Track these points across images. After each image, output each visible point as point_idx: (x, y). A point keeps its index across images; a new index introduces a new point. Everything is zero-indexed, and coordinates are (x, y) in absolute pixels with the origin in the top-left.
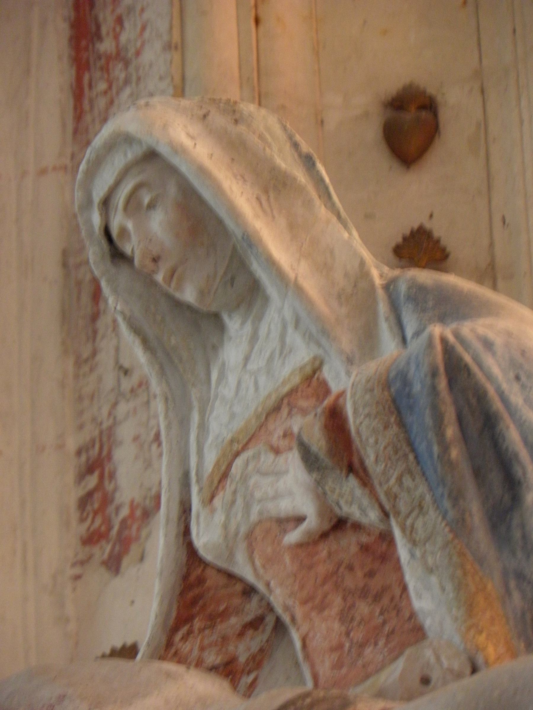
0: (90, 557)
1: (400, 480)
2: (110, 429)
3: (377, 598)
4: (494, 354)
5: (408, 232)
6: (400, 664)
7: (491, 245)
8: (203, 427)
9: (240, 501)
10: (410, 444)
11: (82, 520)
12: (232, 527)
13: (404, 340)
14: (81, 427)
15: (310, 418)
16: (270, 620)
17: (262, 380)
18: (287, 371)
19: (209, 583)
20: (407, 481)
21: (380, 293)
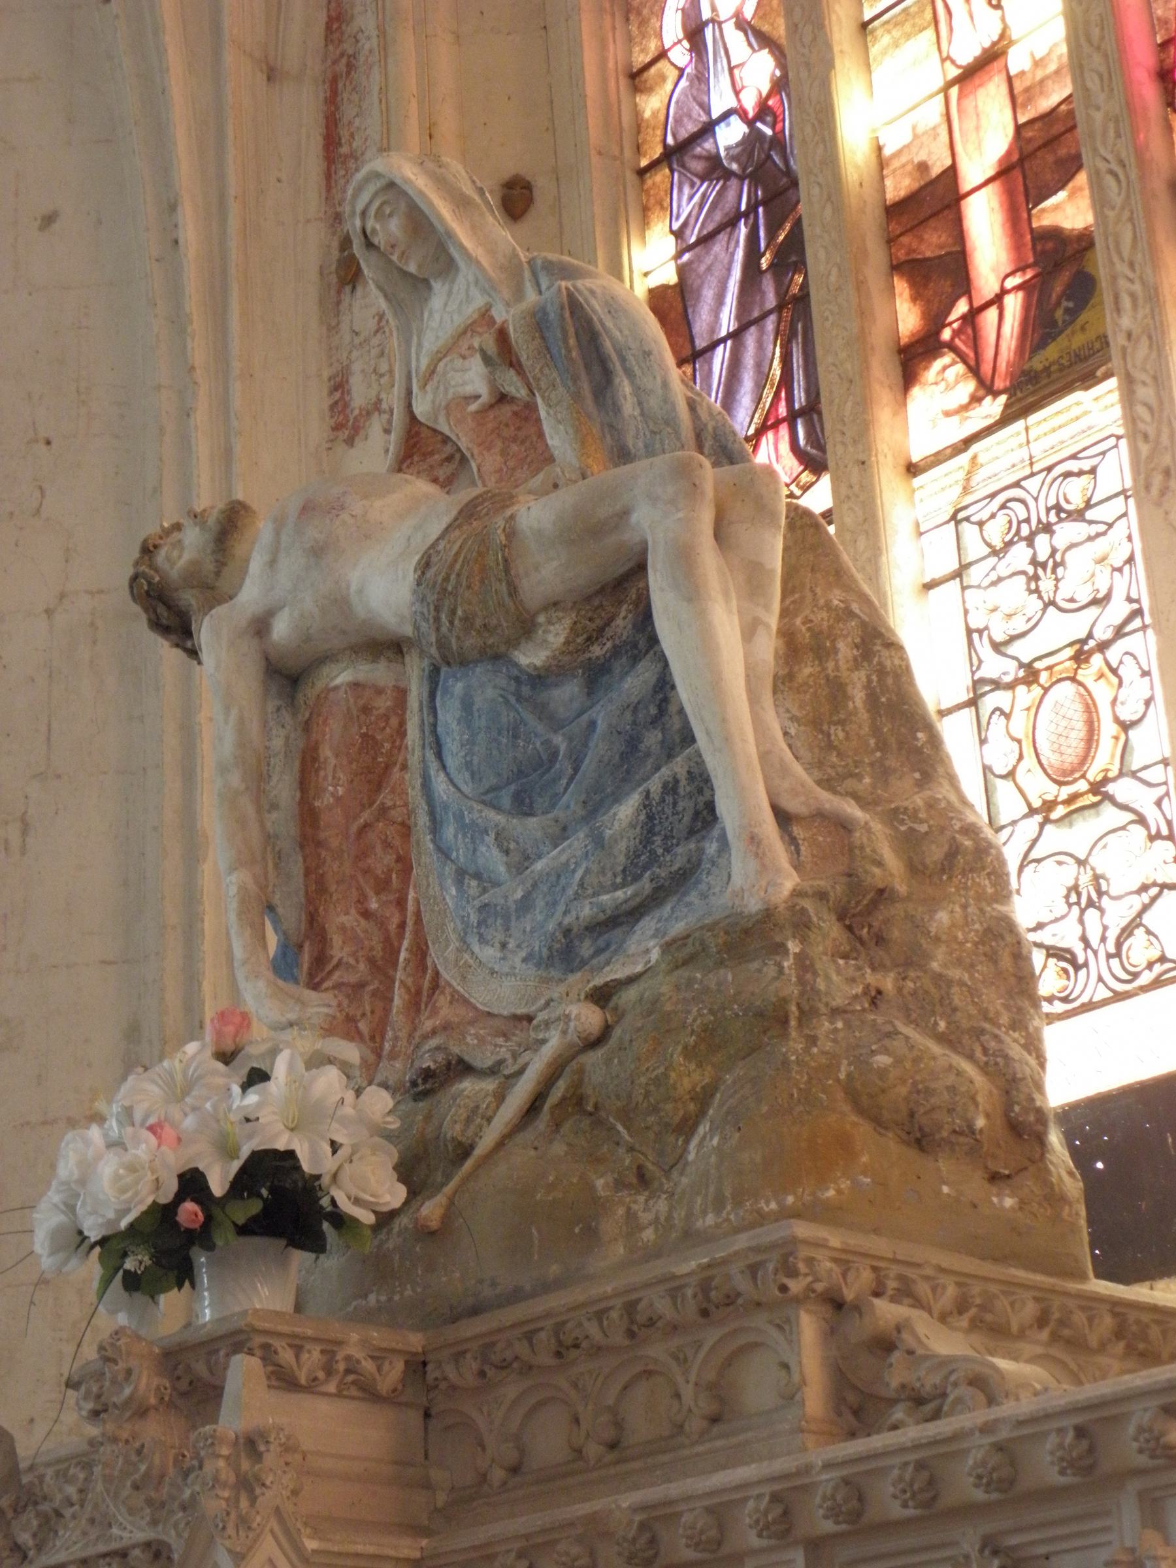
0: (337, 437)
1: (541, 370)
2: (348, 366)
3: (523, 442)
4: (596, 298)
6: (541, 476)
8: (420, 345)
9: (442, 387)
10: (548, 349)
11: (332, 417)
12: (437, 403)
13: (540, 293)
14: (331, 365)
15: (486, 336)
16: (458, 456)
17: (456, 317)
18: (470, 310)
19: (423, 435)
20: (546, 371)
21: (526, 266)
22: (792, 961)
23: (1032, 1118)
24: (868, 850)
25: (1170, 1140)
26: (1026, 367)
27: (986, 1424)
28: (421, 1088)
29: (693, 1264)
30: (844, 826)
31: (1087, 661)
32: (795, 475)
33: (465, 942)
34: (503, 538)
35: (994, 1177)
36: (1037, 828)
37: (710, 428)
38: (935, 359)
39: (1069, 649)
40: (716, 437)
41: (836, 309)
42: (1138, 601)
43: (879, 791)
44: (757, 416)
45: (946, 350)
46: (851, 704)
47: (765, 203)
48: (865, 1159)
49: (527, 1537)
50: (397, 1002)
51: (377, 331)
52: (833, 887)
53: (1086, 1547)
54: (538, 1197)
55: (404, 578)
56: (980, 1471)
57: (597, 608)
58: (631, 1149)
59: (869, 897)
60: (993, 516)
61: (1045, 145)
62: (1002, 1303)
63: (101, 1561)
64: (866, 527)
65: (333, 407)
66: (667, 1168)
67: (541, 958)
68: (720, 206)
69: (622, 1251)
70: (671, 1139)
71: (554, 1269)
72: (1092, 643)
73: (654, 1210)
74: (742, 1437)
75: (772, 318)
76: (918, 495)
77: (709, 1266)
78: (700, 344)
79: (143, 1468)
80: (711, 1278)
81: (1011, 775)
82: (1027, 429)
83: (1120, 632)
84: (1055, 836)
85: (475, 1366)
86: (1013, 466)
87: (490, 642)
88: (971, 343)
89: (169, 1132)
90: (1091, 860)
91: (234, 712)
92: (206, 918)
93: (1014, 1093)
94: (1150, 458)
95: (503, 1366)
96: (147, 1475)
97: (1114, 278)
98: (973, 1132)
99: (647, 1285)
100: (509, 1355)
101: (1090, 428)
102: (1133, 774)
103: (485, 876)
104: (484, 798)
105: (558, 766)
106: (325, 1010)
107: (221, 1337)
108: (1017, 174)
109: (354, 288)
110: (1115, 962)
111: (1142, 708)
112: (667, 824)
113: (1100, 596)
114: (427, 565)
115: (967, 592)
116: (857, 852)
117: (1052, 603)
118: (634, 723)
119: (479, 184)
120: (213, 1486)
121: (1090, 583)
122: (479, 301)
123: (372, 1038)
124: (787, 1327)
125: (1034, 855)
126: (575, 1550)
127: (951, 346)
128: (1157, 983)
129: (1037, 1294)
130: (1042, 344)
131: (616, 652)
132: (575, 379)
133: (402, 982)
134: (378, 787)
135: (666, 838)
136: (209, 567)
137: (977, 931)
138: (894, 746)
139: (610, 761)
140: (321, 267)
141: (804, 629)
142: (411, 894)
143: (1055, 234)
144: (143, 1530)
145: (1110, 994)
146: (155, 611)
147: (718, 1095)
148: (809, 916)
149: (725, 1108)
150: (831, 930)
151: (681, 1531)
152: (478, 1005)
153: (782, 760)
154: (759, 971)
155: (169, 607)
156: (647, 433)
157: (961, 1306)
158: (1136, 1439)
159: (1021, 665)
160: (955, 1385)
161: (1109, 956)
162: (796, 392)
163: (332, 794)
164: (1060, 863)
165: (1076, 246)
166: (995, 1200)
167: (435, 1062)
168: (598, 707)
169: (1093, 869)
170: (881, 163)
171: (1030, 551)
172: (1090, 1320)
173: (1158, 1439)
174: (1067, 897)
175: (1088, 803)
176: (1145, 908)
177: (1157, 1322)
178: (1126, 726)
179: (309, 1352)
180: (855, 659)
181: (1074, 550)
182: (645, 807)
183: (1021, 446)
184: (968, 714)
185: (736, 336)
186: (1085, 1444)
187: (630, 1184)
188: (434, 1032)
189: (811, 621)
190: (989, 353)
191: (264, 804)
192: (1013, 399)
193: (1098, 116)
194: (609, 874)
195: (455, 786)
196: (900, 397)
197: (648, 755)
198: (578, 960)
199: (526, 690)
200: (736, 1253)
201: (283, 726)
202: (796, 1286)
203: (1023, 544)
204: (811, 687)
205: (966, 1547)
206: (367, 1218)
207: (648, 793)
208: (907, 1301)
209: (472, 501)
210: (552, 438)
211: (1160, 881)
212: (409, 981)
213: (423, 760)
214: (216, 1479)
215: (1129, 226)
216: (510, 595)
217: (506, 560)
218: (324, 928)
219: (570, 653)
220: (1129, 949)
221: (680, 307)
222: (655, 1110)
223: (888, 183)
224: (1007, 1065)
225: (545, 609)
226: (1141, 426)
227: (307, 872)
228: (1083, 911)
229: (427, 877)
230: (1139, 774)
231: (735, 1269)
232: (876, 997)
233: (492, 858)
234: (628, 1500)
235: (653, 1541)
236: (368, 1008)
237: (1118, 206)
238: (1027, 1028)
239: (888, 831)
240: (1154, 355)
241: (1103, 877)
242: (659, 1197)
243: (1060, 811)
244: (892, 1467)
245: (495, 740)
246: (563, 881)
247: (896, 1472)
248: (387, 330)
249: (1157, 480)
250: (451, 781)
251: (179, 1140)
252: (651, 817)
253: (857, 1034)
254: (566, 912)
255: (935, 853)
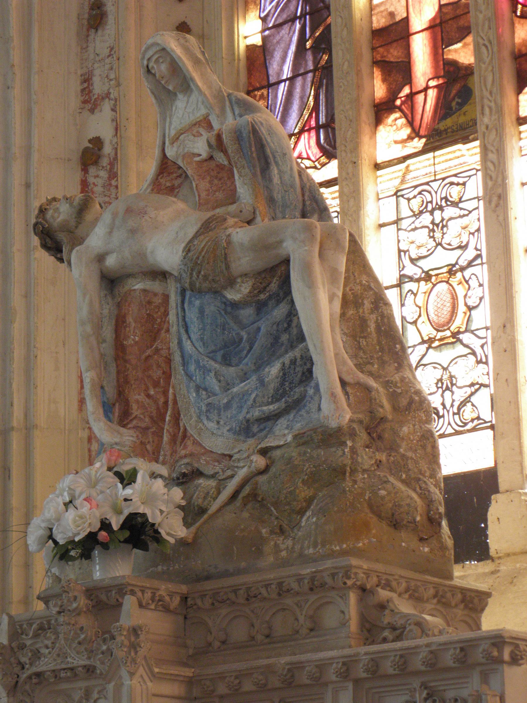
1: (238, 159)
4: (263, 126)
5: (180, 22)
7: (203, 28)
8: (170, 123)
9: (182, 146)
10: (241, 149)
11: (82, 96)
16: (184, 175)
17: (191, 115)
18: (198, 115)
20: (240, 159)
21: (226, 98)
22: (348, 449)
23: (437, 517)
24: (378, 401)
25: (475, 500)
26: (436, 127)
27: (428, 644)
28: (181, 481)
29: (308, 571)
30: (368, 389)
31: (454, 274)
32: (318, 157)
33: (200, 418)
34: (225, 244)
35: (421, 539)
36: (425, 350)
37: (308, 186)
38: (392, 114)
39: (446, 268)
40: (310, 191)
41: (346, 83)
42: (480, 250)
43: (381, 372)
44: (300, 123)
45: (397, 110)
46: (369, 329)
47: (310, 14)
48: (374, 531)
49: (240, 671)
50: (165, 439)
51: (109, 56)
52: (365, 419)
53: (459, 688)
54: (237, 534)
55: (177, 253)
56: (424, 660)
57: (263, 279)
58: (277, 518)
59: (377, 421)
60: (415, 197)
61: (453, 18)
62: (421, 589)
63: (62, 671)
64: (354, 194)
65: (83, 90)
66: (292, 527)
67: (236, 431)
68: (286, 11)
69: (272, 559)
70: (295, 516)
71: (243, 564)
72: (457, 267)
73: (286, 544)
74: (324, 638)
75: (310, 75)
76: (379, 180)
77: (315, 572)
78: (272, 80)
79: (83, 636)
80: (315, 577)
81: (415, 323)
82: (434, 157)
83: (470, 264)
84: (433, 356)
85: (210, 601)
86: (426, 174)
87: (214, 286)
88: (410, 109)
89: (94, 503)
90: (449, 368)
91: (88, 296)
92: (15, 351)
93: (431, 506)
94: (492, 188)
95: (223, 602)
96: (84, 639)
97: (482, 98)
98: (415, 522)
99: (289, 577)
100: (225, 598)
101: (464, 163)
102: (472, 332)
103: (209, 390)
104: (209, 355)
105: (242, 345)
106: (131, 439)
107: (114, 586)
108: (438, 29)
109: (97, 30)
110: (457, 417)
111: (478, 301)
112: (291, 377)
113: (463, 245)
114: (189, 250)
115: (400, 232)
116: (373, 401)
117: (440, 244)
118: (278, 330)
119: (202, 50)
120: (121, 646)
121: (459, 238)
122: (203, 111)
123: (154, 453)
124: (344, 597)
125: (422, 362)
126: (261, 677)
127: (400, 109)
128: (474, 429)
129: (434, 586)
130: (444, 117)
131: (270, 297)
132: (254, 167)
133: (167, 430)
134: (154, 339)
135: (290, 383)
136: (73, 223)
137: (418, 436)
138: (387, 350)
139: (266, 346)
140: (78, 14)
141: (350, 293)
142: (171, 391)
143: (454, 64)
144: (84, 661)
145: (454, 431)
146: (45, 241)
147: (316, 501)
148: (356, 431)
149: (318, 507)
150: (363, 436)
151: (305, 672)
152: (206, 447)
153: (343, 358)
154: (335, 452)
155: (51, 239)
156: (283, 191)
157: (407, 590)
158: (482, 653)
159: (423, 272)
160: (410, 624)
161: (454, 414)
162: (321, 115)
163: (133, 340)
164: (435, 368)
165: (464, 72)
166: (421, 548)
167: (187, 470)
168: (261, 322)
169: (450, 372)
170: (371, 8)
171: (431, 218)
172: (453, 595)
173: (490, 654)
174: (437, 384)
175: (450, 341)
176: (472, 394)
177: (477, 596)
178: (470, 309)
179: (147, 593)
180: (372, 309)
181: (452, 221)
182: (283, 370)
183: (430, 165)
184: (396, 290)
185: (292, 79)
186: (463, 653)
187: (277, 532)
188: (185, 456)
189: (353, 290)
190: (418, 117)
191: (101, 341)
192: (428, 142)
193: (481, 16)
194: (266, 397)
195: (195, 347)
196: (373, 129)
197: (282, 344)
198: (251, 433)
199: (229, 309)
200: (327, 568)
201: (108, 304)
202: (349, 583)
203: (428, 214)
204: (352, 320)
205: (415, 685)
206: (172, 540)
207: (284, 364)
208: (388, 588)
209: (207, 220)
210: (240, 189)
211: (480, 382)
212: (171, 430)
213: (179, 331)
214: (122, 644)
215: (491, 74)
216: (226, 269)
217: (226, 254)
218: (127, 400)
219: (251, 297)
220: (464, 411)
221: (262, 59)
222: (289, 504)
223: (374, 18)
224: (429, 494)
225: (241, 276)
226: (489, 172)
227: (118, 372)
228: (444, 392)
229: (180, 385)
230: (475, 332)
231: (325, 574)
232: (379, 464)
233: (212, 382)
234: (284, 660)
235: (293, 676)
236: (151, 440)
237: (487, 63)
238: (436, 477)
239: (386, 392)
240: (498, 139)
241: (454, 377)
242: (289, 539)
243: (436, 344)
244: (390, 656)
245: (214, 330)
246: (245, 397)
247: (392, 658)
248: (114, 56)
249: (495, 199)
250: (193, 345)
251: (98, 505)
252: (284, 374)
253: (372, 480)
254: (248, 413)
255: (404, 402)
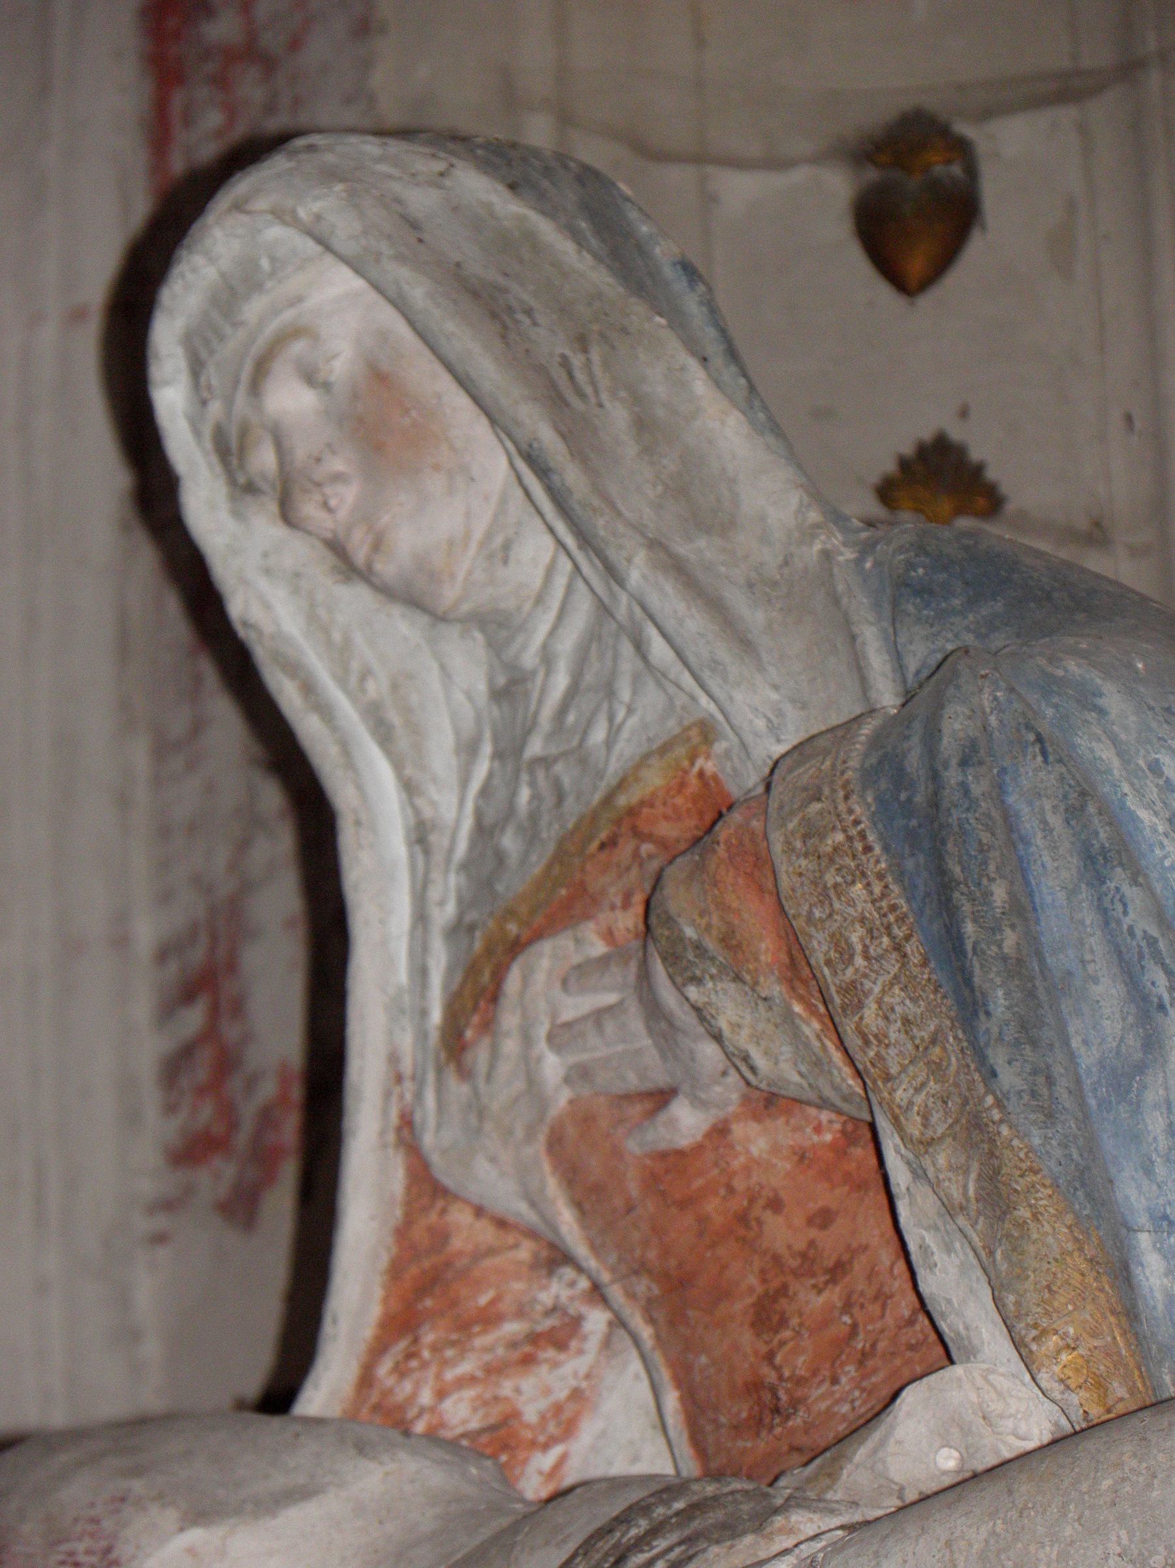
0: (189, 1191)
11: (170, 1109)
